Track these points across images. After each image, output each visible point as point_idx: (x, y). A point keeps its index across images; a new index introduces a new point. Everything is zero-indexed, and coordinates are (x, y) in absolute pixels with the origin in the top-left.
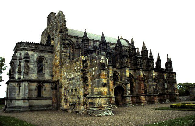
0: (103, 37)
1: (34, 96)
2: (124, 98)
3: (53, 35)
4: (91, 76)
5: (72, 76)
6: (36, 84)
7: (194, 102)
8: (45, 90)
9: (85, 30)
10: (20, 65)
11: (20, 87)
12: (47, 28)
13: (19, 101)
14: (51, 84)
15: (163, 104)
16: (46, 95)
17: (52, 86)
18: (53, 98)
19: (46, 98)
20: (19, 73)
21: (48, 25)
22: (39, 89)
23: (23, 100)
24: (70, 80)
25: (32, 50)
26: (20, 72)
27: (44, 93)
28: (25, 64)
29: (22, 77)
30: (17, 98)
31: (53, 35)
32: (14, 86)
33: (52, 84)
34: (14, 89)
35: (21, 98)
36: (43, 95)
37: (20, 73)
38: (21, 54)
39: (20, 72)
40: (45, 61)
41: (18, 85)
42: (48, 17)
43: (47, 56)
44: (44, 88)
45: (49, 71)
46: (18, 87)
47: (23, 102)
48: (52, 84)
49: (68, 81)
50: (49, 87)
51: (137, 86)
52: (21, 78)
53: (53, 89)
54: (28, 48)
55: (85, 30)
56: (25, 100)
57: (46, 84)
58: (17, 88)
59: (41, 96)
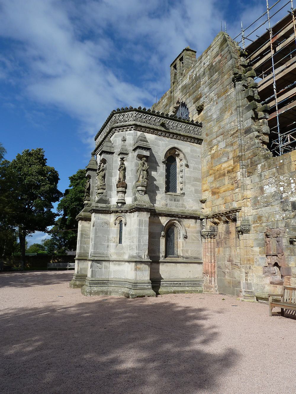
2: (88, 237)
10: (123, 169)
13: (119, 265)
19: (188, 261)
20: (120, 189)
23: (136, 262)
25: (153, 131)
26: (122, 185)
28: (137, 165)
29: (129, 200)
30: (114, 257)
33: (202, 223)
34: (107, 232)
35: (126, 257)
37: (123, 189)
38: (124, 140)
39: (122, 185)
40: (184, 162)
41: (118, 222)
43: (185, 147)
44: (182, 233)
47: (136, 270)
48: (202, 223)
49: (227, 222)
51: (8, 257)
52: (125, 203)
54: (143, 124)
56: (141, 262)
57: (186, 222)
58: (115, 229)
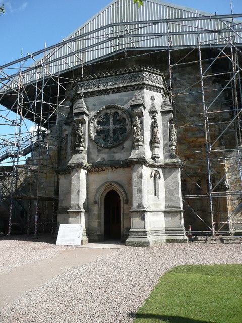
13: (157, 215)
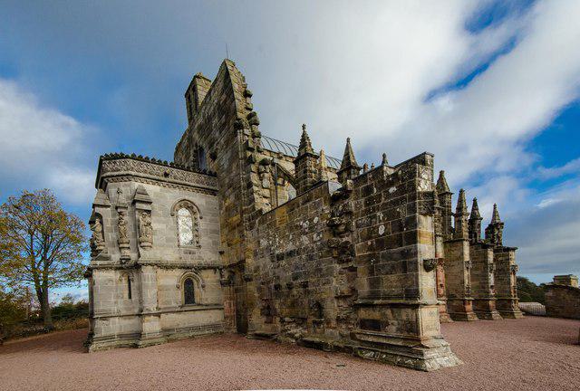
0: (304, 141)
1: (173, 304)
3: (211, 145)
4: (369, 238)
5: (290, 247)
6: (178, 273)
7: (572, 324)
8: (203, 287)
9: (304, 127)
11: (132, 283)
12: (190, 130)
14: (218, 274)
15: (365, 365)
16: (207, 299)
17: (222, 276)
18: (226, 306)
21: (191, 119)
22: (188, 285)
24: (280, 257)
27: (202, 295)
31: (211, 145)
32: (347, 242)
36: (197, 300)
42: (187, 95)
45: (211, 241)
46: (124, 281)
50: (213, 279)
53: (222, 284)
55: (304, 127)
57: (204, 274)
59: (194, 302)
